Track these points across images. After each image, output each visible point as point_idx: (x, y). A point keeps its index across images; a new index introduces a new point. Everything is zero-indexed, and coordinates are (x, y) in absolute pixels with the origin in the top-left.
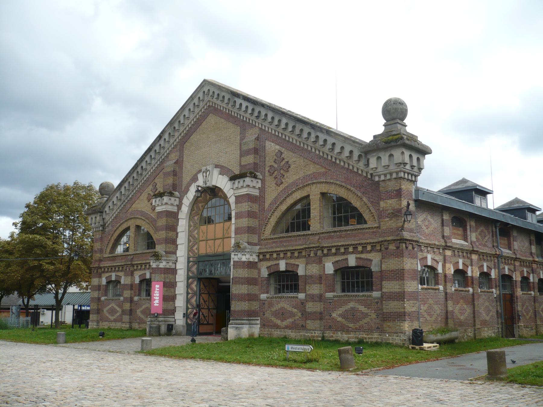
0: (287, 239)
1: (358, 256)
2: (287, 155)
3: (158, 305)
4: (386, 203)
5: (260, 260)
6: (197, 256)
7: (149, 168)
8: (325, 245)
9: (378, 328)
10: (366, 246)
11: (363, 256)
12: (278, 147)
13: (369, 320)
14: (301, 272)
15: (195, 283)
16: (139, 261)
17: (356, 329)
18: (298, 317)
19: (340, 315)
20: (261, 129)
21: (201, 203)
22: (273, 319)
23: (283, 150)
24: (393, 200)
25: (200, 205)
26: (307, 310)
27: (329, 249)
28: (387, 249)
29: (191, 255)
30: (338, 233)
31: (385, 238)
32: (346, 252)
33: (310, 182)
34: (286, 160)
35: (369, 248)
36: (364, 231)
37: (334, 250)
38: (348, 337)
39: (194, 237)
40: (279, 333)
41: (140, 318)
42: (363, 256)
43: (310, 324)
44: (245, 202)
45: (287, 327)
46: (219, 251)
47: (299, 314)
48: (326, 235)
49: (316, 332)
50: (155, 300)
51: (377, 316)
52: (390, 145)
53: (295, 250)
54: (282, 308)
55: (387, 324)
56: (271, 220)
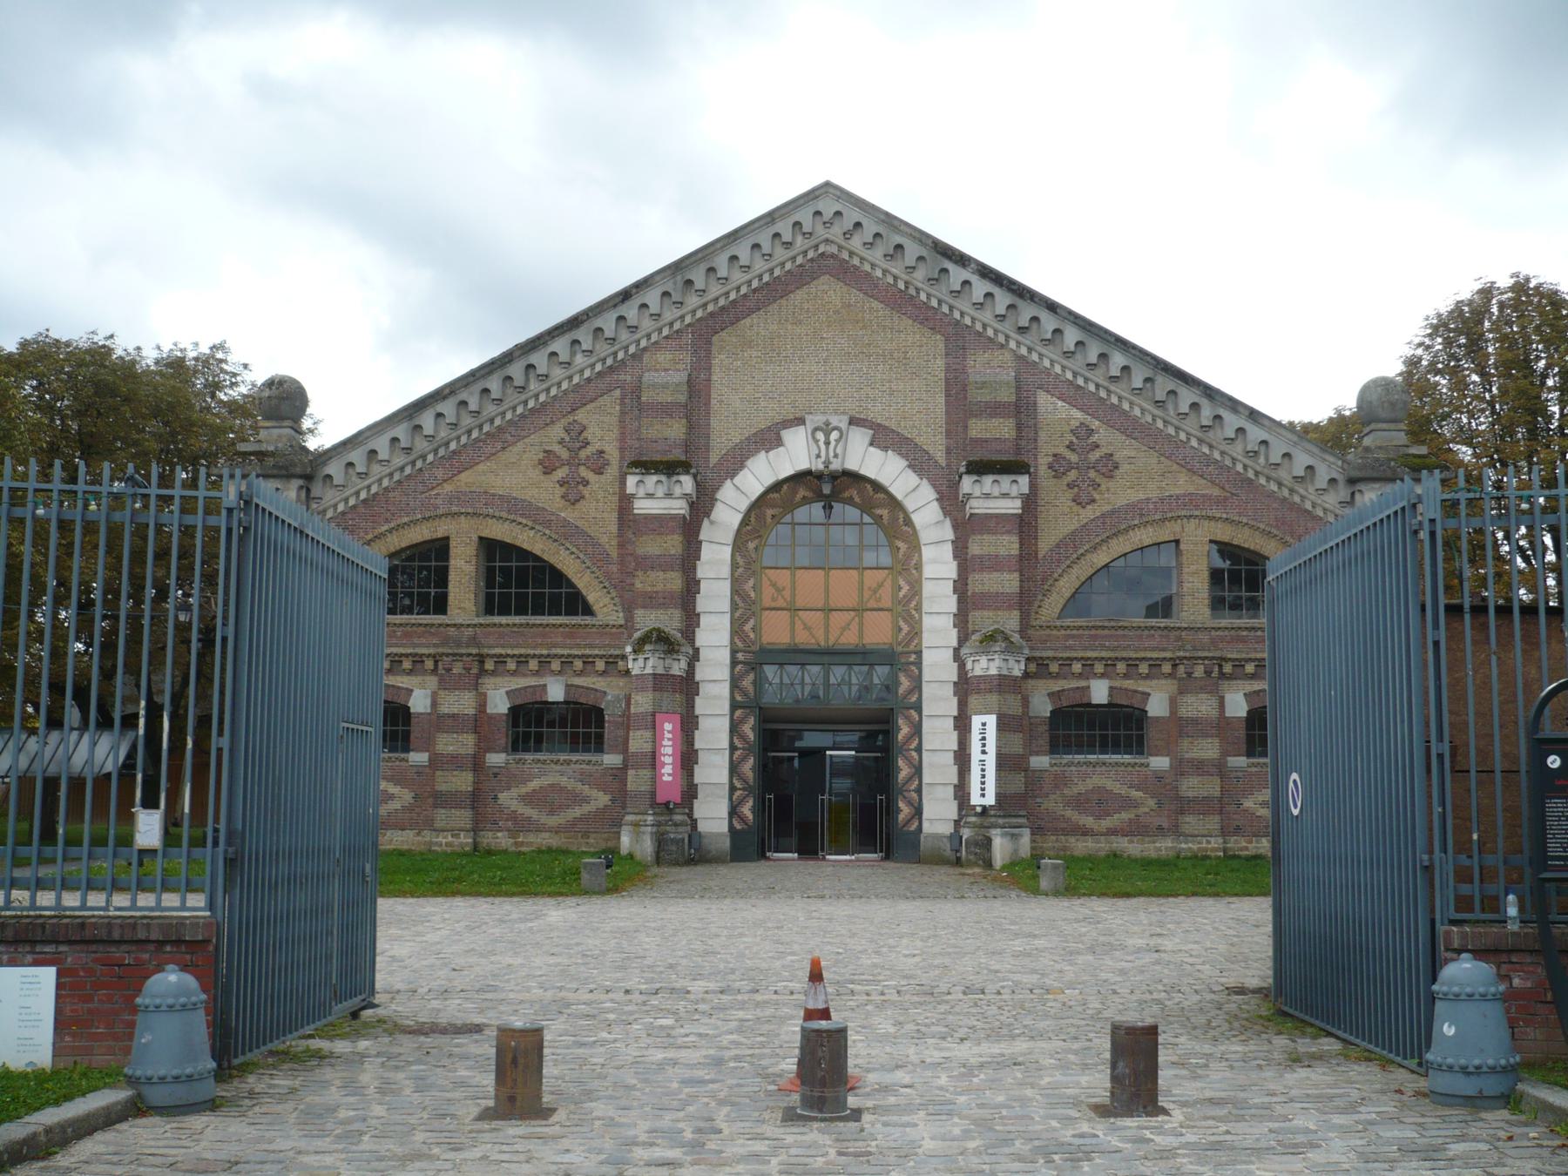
0: (1113, 632)
2: (1105, 437)
5: (1035, 676)
7: (558, 373)
11: (1129, 684)
12: (1077, 414)
14: (1157, 707)
15: (752, 721)
16: (517, 646)
19: (586, 800)
21: (773, 507)
22: (1069, 813)
27: (1239, 664)
28: (449, 670)
29: (740, 644)
33: (1183, 513)
34: (1104, 450)
41: (513, 817)
42: (1129, 684)
43: (1191, 822)
44: (1008, 532)
45: (1112, 832)
46: (843, 640)
47: (1152, 803)
50: (664, 764)
54: (1099, 790)
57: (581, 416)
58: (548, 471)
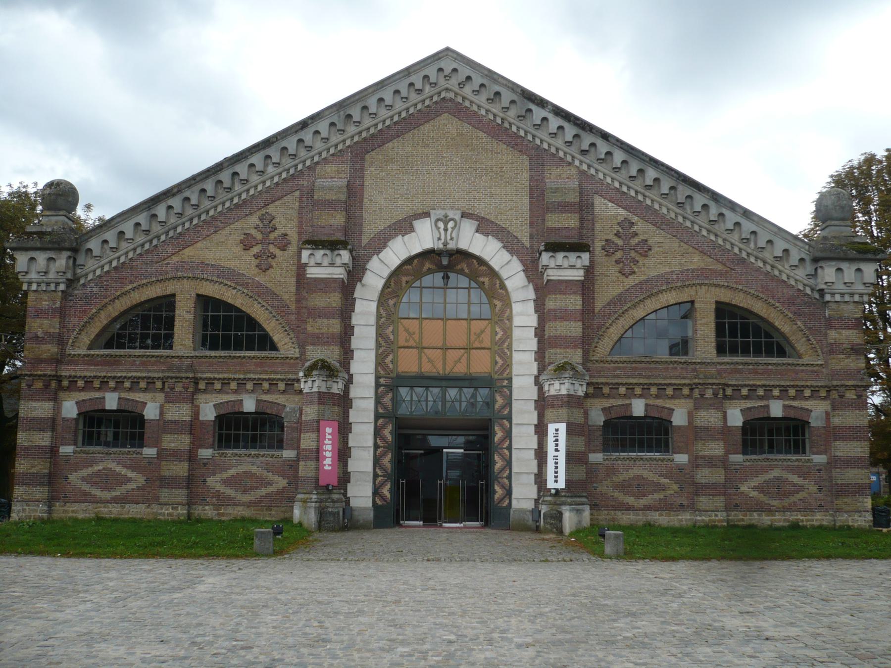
0: (648, 365)
1: (787, 403)
2: (642, 228)
3: (330, 468)
4: (840, 333)
6: (394, 375)
7: (255, 179)
8: (730, 383)
9: (821, 506)
10: (154, 383)
12: (623, 212)
13: (806, 496)
17: (784, 507)
18: (672, 492)
19: (754, 488)
20: (583, 173)
22: (616, 494)
23: (635, 219)
24: (851, 331)
25: (404, 279)
26: (698, 481)
27: (737, 389)
28: (172, 389)
29: (382, 372)
30: (751, 367)
31: (843, 382)
32: (768, 396)
35: (807, 393)
36: (797, 368)
37: (744, 392)
38: (772, 521)
39: (386, 339)
40: (632, 517)
41: (217, 494)
43: (704, 501)
44: (574, 293)
45: (648, 508)
46: (456, 370)
48: (728, 366)
49: (719, 514)
51: (820, 489)
52: (865, 256)
53: (249, 379)
55: (840, 502)
56: (611, 330)
57: (271, 209)
58: (247, 248)
